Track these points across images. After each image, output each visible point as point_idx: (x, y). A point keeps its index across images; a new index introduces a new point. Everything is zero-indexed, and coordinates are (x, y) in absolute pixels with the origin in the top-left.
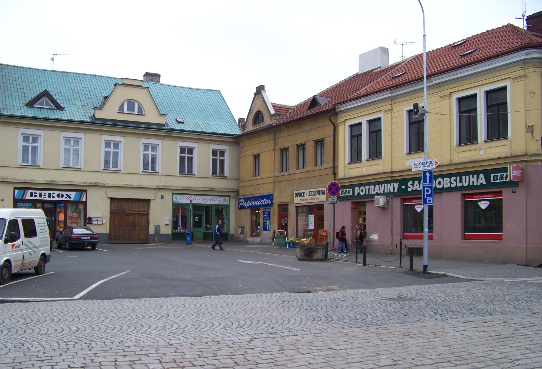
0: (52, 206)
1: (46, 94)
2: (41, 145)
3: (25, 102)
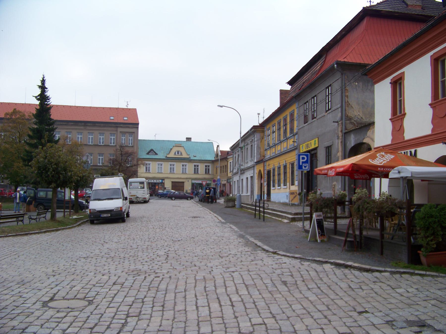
2: (175, 167)
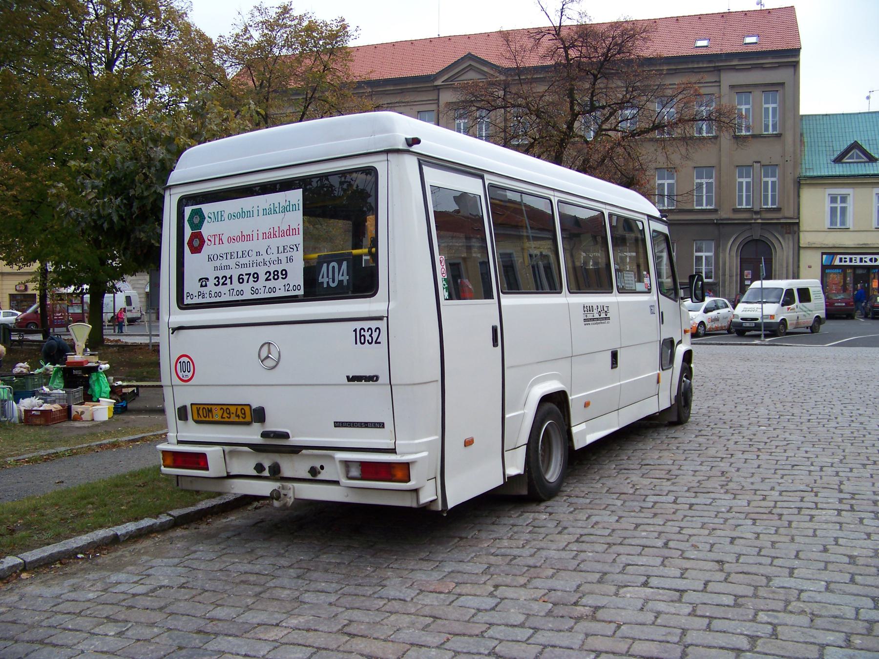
0: (865, 272)
1: (855, 146)
2: (850, 205)
3: (833, 158)
